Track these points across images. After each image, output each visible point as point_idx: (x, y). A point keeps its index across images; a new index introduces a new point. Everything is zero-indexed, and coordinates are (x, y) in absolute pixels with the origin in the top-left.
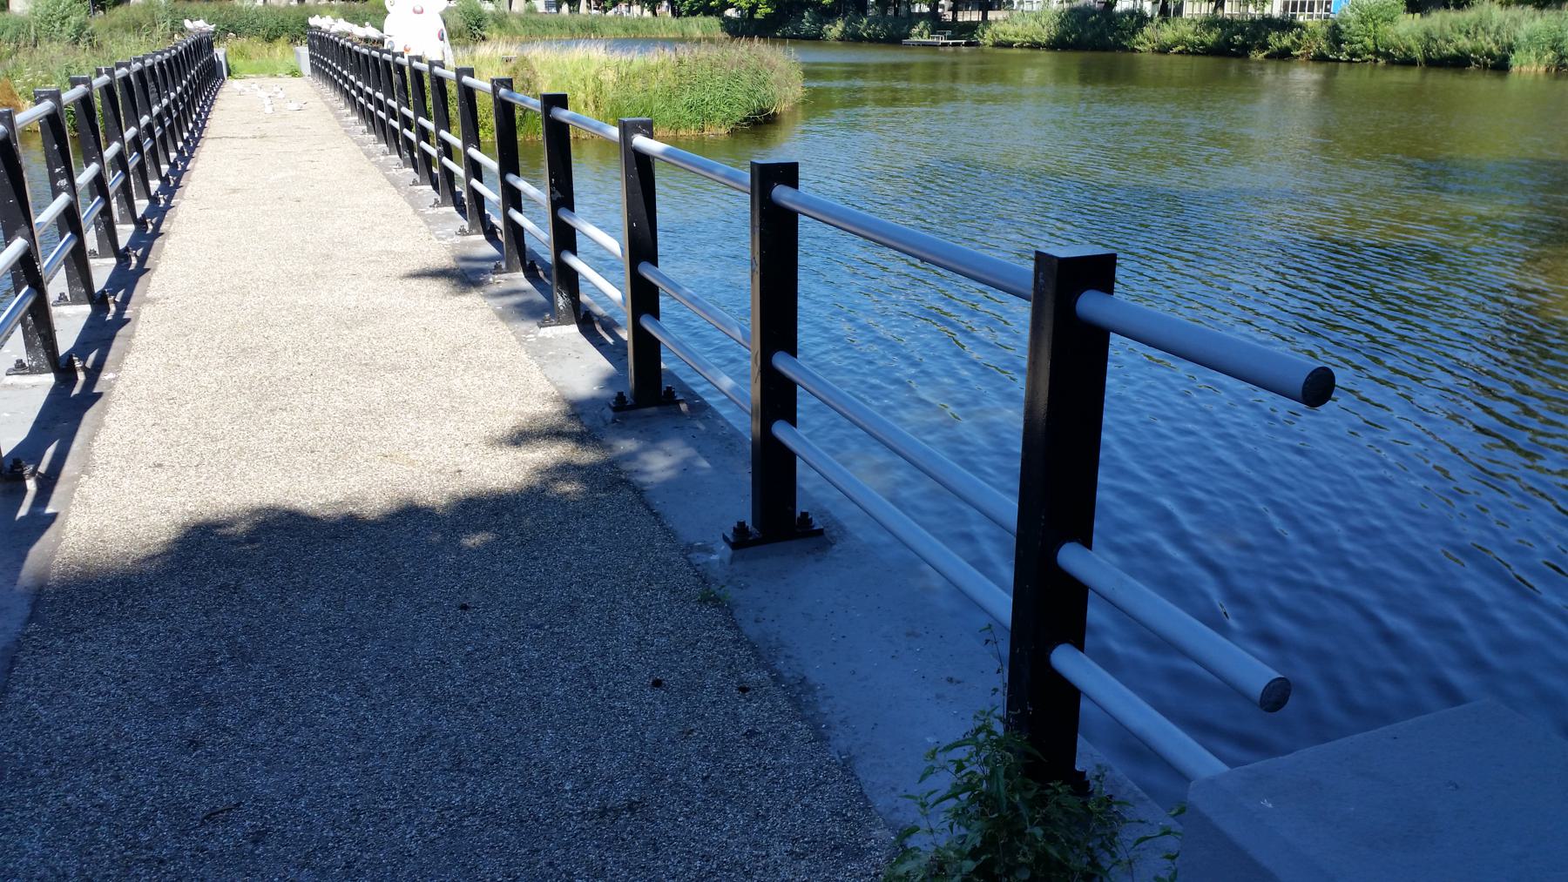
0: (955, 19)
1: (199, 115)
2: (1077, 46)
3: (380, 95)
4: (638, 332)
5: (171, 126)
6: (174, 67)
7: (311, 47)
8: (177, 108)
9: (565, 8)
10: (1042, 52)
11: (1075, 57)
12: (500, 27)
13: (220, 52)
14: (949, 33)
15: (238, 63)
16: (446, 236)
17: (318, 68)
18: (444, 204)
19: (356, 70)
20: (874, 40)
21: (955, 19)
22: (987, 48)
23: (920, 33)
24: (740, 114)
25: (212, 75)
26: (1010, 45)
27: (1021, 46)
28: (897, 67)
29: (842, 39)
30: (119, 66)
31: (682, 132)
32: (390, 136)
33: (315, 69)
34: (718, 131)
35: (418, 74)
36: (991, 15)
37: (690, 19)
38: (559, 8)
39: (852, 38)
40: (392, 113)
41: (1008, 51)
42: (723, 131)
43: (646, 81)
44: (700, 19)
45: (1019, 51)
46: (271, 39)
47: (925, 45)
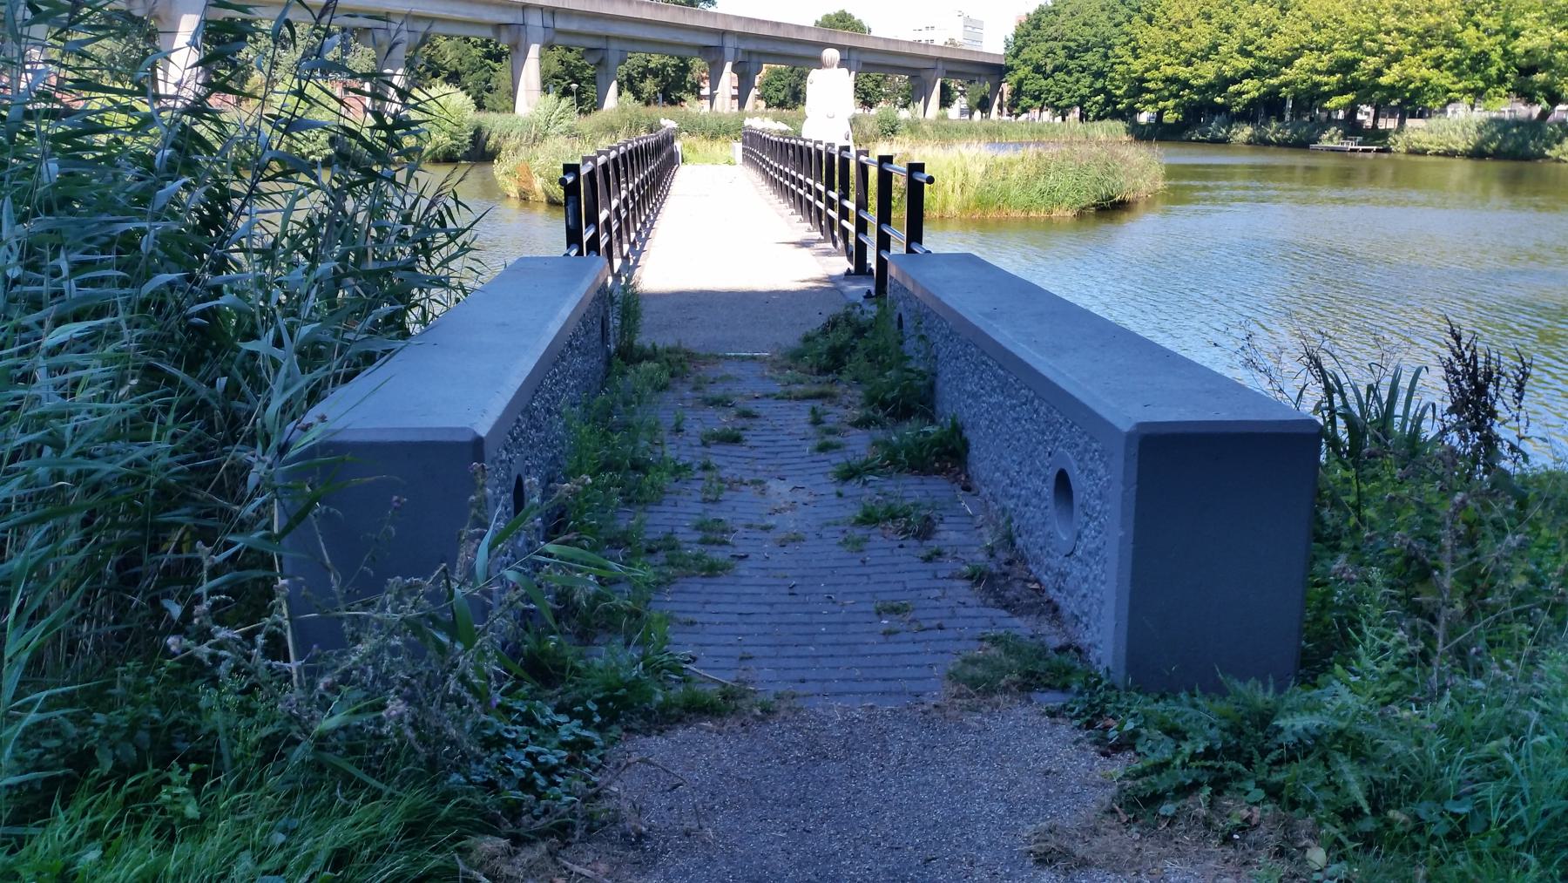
0: (1375, 126)
1: (644, 224)
2: (1497, 155)
3: (801, 177)
4: (858, 241)
5: (627, 218)
6: (633, 159)
7: (744, 142)
8: (633, 198)
9: (977, 114)
10: (1458, 161)
11: (1491, 166)
12: (912, 131)
13: (678, 145)
14: (1359, 138)
15: (689, 155)
16: (803, 229)
17: (749, 158)
18: (825, 241)
19: (772, 154)
20: (1283, 144)
21: (1375, 126)
22: (1402, 157)
23: (1331, 139)
24: (1088, 199)
25: (672, 161)
26: (1423, 152)
27: (1437, 154)
28: (1263, 167)
29: (1249, 143)
30: (600, 153)
31: (1032, 214)
32: (785, 192)
33: (745, 158)
34: (1065, 213)
35: (819, 153)
36: (1409, 122)
37: (1097, 123)
38: (971, 114)
39: (1259, 142)
40: (800, 183)
41: (1421, 159)
42: (1069, 214)
43: (1006, 171)
44: (1108, 123)
45: (1433, 159)
46: (714, 137)
47: (1333, 150)
